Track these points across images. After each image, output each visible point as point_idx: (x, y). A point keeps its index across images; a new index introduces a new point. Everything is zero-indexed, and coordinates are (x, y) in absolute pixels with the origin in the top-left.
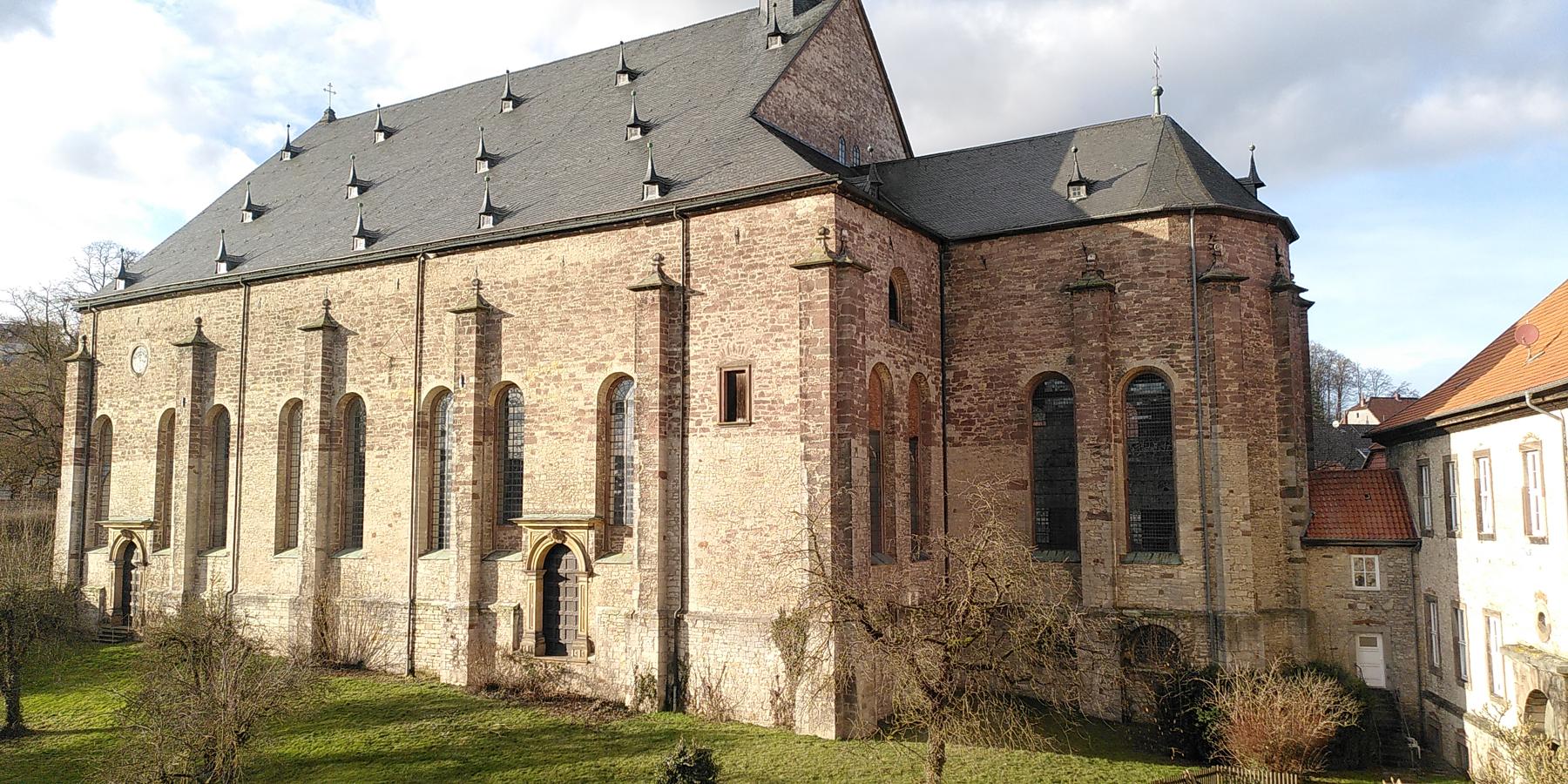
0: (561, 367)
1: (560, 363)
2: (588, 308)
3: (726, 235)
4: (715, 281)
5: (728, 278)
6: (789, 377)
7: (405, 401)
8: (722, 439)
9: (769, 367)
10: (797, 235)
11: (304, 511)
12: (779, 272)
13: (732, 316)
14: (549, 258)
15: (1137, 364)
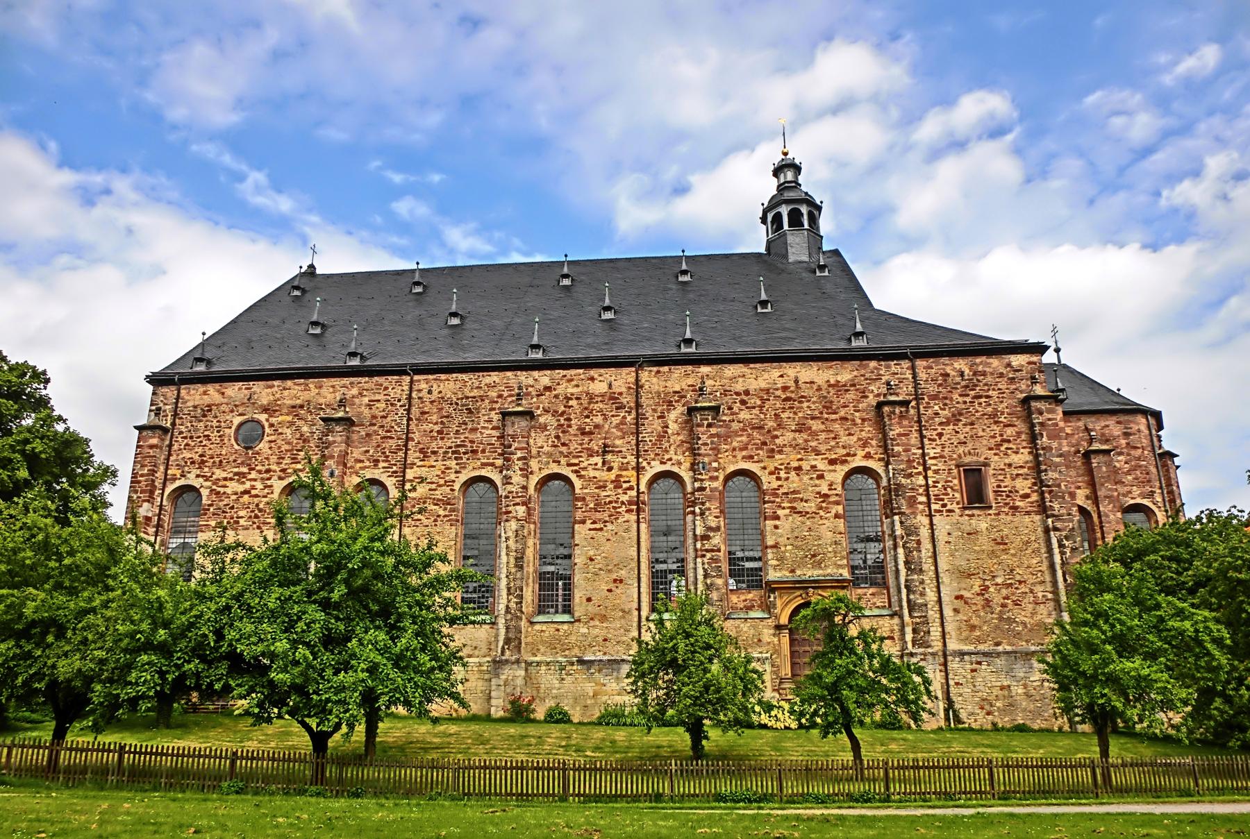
0: (801, 460)
1: (799, 456)
2: (826, 416)
3: (952, 373)
4: (945, 405)
5: (958, 403)
6: (1021, 475)
7: (625, 482)
8: (967, 518)
9: (1002, 467)
10: (1014, 378)
11: (507, 577)
12: (1002, 402)
13: (965, 430)
14: (781, 376)
15: (1132, 502)
